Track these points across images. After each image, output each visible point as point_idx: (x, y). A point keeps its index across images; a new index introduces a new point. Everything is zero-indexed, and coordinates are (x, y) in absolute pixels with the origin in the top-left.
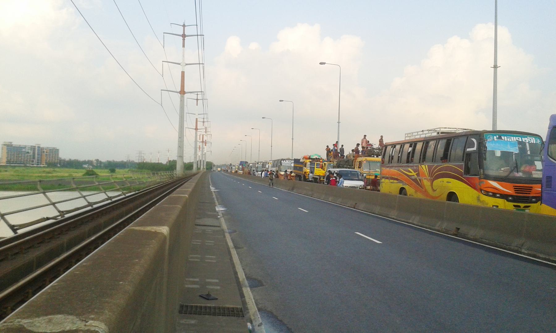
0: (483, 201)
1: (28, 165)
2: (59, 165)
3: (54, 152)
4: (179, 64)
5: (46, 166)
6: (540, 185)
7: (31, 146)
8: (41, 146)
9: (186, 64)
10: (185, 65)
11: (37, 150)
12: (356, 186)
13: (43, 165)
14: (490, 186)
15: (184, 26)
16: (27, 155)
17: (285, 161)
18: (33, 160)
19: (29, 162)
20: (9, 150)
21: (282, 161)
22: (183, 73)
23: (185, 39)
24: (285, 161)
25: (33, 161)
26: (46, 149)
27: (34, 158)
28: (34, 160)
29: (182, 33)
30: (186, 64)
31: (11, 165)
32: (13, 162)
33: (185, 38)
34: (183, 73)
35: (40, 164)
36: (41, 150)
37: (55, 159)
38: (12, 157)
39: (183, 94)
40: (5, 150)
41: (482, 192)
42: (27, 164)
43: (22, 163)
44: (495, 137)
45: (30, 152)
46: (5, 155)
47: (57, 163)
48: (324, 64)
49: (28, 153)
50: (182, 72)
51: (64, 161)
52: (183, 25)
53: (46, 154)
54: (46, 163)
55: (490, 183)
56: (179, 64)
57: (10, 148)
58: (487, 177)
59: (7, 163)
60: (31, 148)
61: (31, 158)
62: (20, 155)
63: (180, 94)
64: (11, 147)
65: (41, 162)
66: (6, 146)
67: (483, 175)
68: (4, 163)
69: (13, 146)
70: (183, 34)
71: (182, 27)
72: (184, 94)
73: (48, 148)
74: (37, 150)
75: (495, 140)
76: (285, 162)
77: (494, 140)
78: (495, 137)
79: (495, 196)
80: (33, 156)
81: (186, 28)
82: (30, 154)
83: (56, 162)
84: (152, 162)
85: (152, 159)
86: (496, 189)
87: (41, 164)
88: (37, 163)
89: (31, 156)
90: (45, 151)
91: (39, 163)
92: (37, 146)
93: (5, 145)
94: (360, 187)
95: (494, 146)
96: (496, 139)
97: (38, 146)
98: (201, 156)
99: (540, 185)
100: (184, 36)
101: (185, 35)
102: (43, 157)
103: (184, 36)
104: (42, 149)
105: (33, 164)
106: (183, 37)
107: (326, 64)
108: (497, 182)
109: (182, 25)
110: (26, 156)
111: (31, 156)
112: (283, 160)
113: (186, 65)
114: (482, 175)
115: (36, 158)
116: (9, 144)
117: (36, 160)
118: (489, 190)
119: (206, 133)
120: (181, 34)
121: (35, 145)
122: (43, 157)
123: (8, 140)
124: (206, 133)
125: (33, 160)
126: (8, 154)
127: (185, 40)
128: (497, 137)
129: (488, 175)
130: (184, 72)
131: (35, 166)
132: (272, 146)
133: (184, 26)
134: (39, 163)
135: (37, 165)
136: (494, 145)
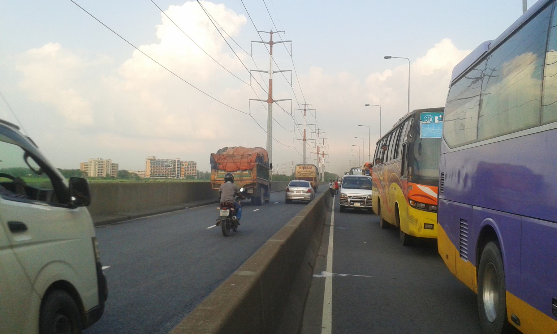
0: (411, 216)
1: (169, 178)
2: (197, 177)
3: (192, 165)
4: (267, 72)
5: (185, 178)
6: (437, 187)
7: (172, 160)
8: (181, 160)
9: (274, 72)
10: (273, 73)
11: (177, 163)
12: (362, 196)
13: (183, 177)
14: (420, 194)
15: (271, 33)
16: (169, 168)
17: (356, 169)
18: (174, 173)
19: (170, 175)
20: (153, 164)
21: (353, 170)
22: (271, 81)
23: (272, 47)
24: (356, 169)
25: (173, 174)
26: (185, 163)
27: (174, 171)
28: (175, 173)
29: (269, 40)
30: (274, 72)
31: (154, 177)
32: (156, 175)
33: (273, 46)
34: (271, 81)
35: (180, 176)
36: (180, 163)
37: (188, 172)
38: (155, 170)
39: (271, 103)
40: (149, 164)
41: (409, 202)
42: (168, 177)
43: (164, 175)
44: (436, 118)
45: (171, 165)
46: (149, 169)
47: (195, 176)
48: (390, 58)
49: (169, 166)
50: (270, 80)
51: (202, 173)
52: (270, 32)
53: (185, 167)
54: (185, 175)
55: (418, 188)
56: (267, 72)
57: (153, 162)
58: (419, 180)
59: (150, 176)
60: (172, 162)
61: (172, 171)
62: (162, 169)
63: (268, 102)
64: (155, 161)
65: (181, 175)
66: (149, 160)
67: (411, 175)
68: (148, 176)
69: (156, 160)
70: (270, 42)
71: (270, 34)
72: (272, 103)
73: (187, 161)
74: (177, 163)
75: (436, 121)
76: (357, 171)
77: (434, 122)
78: (436, 118)
79: (428, 209)
80: (174, 169)
81: (273, 35)
82: (171, 167)
83: (194, 174)
84: (278, 174)
85: (278, 172)
86: (432, 199)
87: (180, 177)
88: (178, 175)
89: (172, 169)
90: (184, 164)
91: (179, 175)
92: (177, 160)
93: (149, 159)
94: (369, 198)
95: (433, 131)
96: (438, 121)
97: (179, 160)
98: (321, 168)
99: (437, 187)
100: (271, 43)
101: (272, 42)
102: (183, 170)
103: (271, 43)
104: (182, 162)
105: (174, 177)
106: (270, 44)
107: (392, 58)
108: (430, 188)
109: (270, 32)
110: (167, 169)
111: (172, 169)
112: (355, 168)
113: (273, 73)
114: (410, 177)
115: (176, 171)
116: (153, 158)
117: (177, 173)
118: (419, 199)
119: (323, 144)
120: (269, 42)
121: (175, 159)
122: (183, 170)
123: (151, 156)
124: (323, 144)
125: (174, 173)
126: (152, 168)
127: (273, 48)
128: (439, 117)
129: (422, 176)
130: (272, 80)
131: (176, 178)
132: (370, 155)
133: (271, 33)
134: (179, 175)
135: (178, 177)
136: (433, 129)
